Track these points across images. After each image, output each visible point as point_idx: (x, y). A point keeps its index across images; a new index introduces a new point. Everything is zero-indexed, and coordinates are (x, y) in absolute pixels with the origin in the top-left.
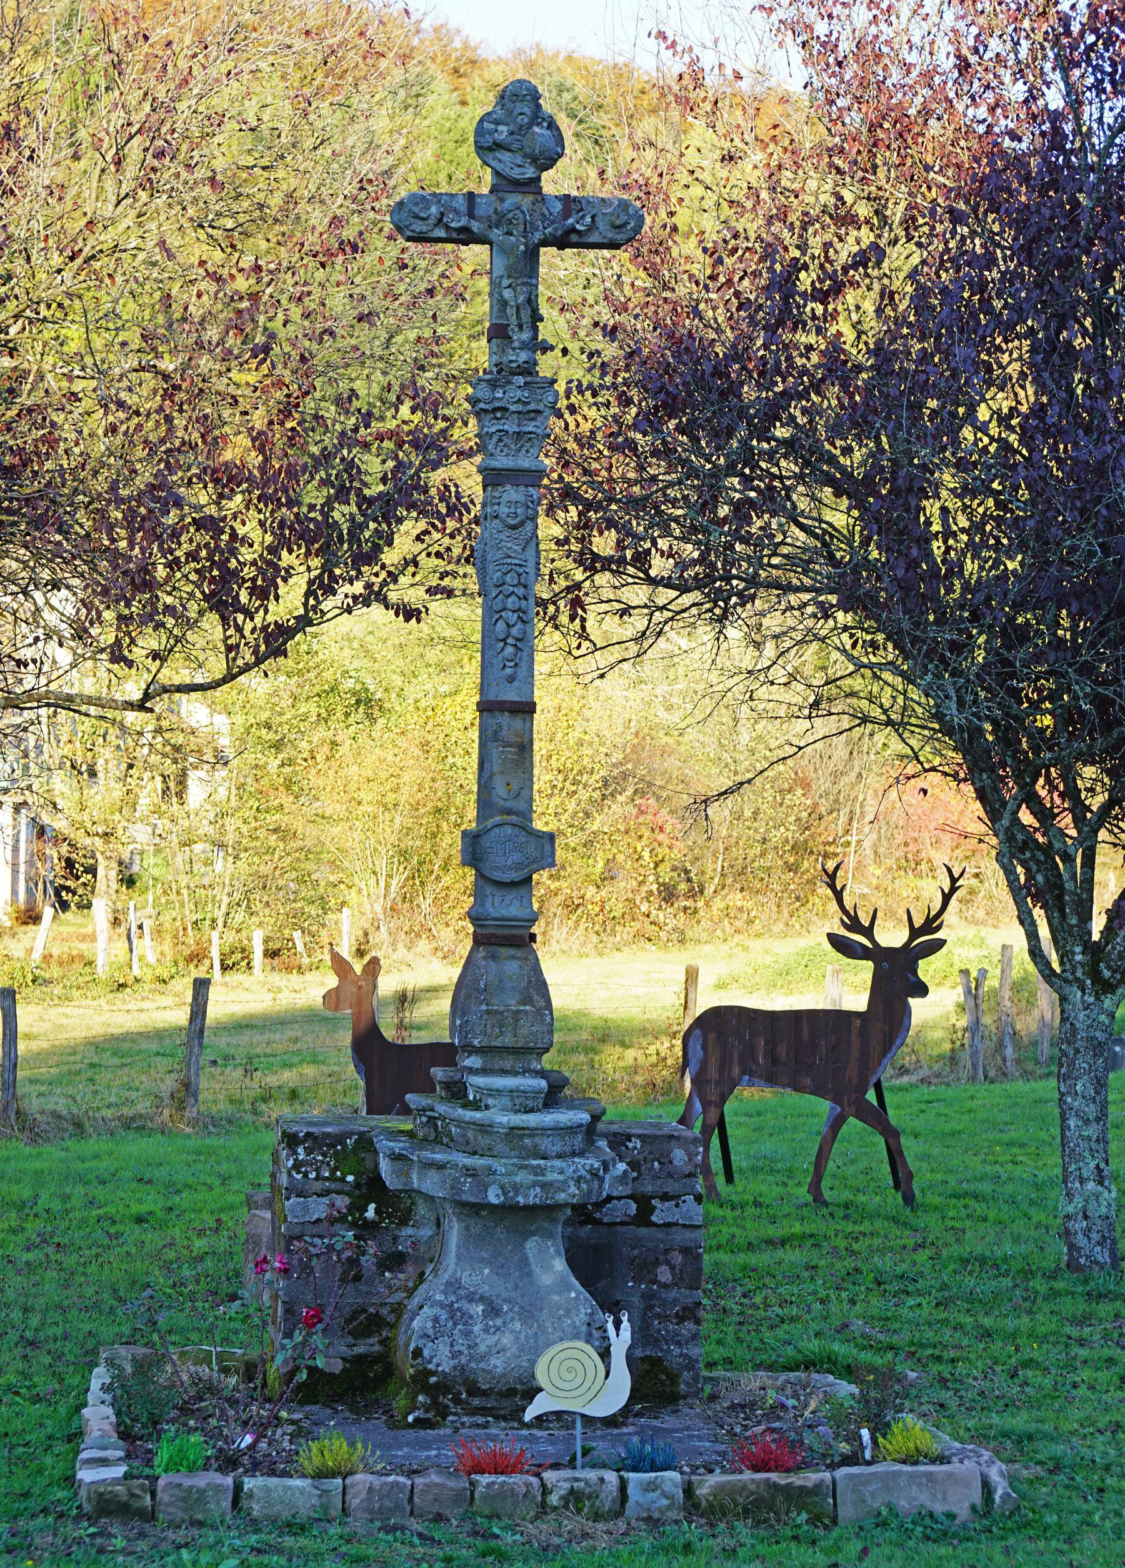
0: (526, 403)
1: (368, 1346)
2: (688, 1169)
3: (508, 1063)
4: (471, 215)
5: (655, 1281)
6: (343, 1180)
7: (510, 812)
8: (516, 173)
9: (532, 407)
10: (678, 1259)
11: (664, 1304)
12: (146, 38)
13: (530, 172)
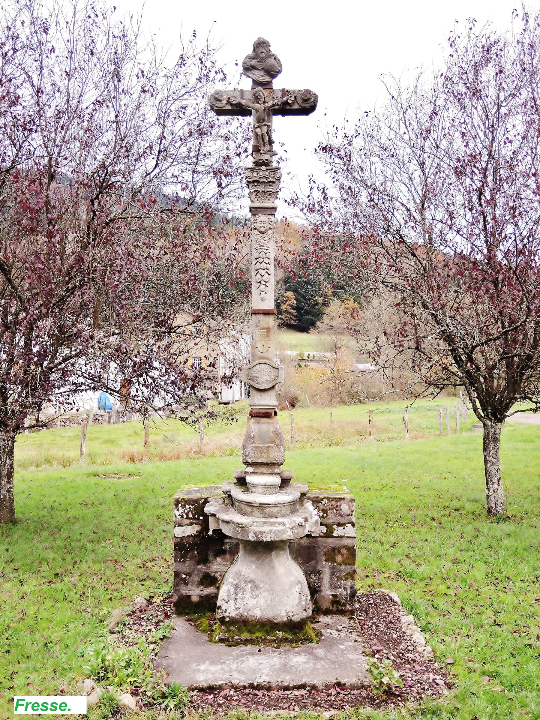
0: (267, 178)
1: (209, 591)
2: (349, 512)
3: (264, 470)
4: (242, 97)
5: (335, 562)
6: (198, 518)
7: (263, 358)
8: (261, 79)
9: (270, 180)
10: (344, 551)
11: (340, 571)
12: (534, 582)
13: (267, 79)
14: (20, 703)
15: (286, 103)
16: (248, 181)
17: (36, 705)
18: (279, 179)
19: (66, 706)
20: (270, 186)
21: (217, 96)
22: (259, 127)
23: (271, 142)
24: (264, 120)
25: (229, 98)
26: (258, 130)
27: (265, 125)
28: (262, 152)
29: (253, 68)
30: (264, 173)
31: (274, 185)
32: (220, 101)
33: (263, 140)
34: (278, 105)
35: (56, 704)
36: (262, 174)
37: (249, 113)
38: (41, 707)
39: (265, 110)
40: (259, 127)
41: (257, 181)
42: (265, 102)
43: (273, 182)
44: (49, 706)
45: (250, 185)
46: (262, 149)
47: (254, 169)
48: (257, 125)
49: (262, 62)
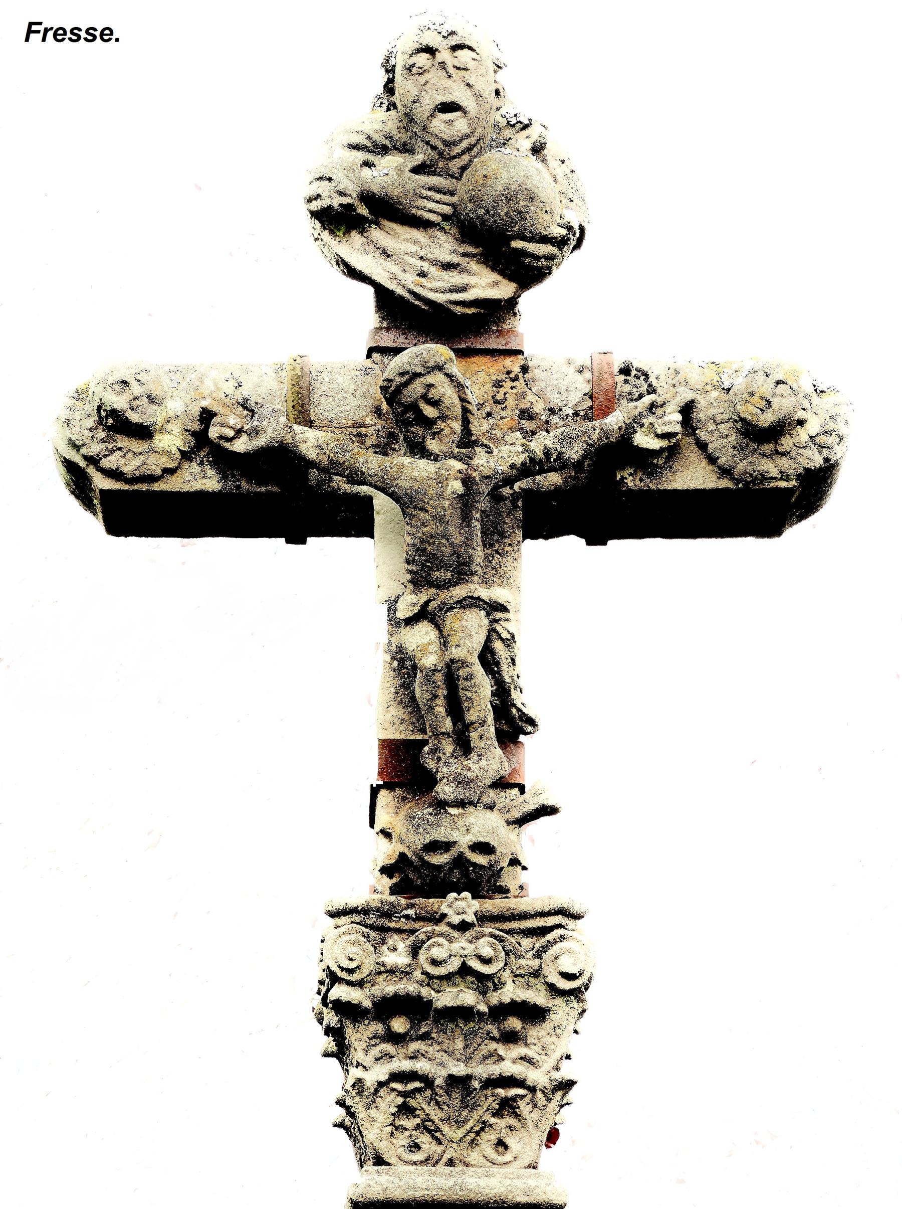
0: (485, 983)
8: (437, 288)
9: (510, 992)
13: (486, 284)
14: (34, 28)
15: (620, 451)
16: (340, 1007)
17: (61, 32)
18: (574, 990)
19: (112, 33)
20: (510, 1038)
21: (119, 402)
22: (423, 614)
23: (512, 726)
24: (462, 571)
25: (207, 416)
26: (421, 637)
27: (472, 602)
28: (445, 790)
29: (383, 209)
30: (462, 945)
31: (535, 1033)
32: (144, 432)
33: (456, 708)
34: (561, 464)
35: (95, 30)
36: (450, 950)
37: (355, 520)
38: (69, 35)
39: (466, 501)
40: (423, 614)
41: (414, 1007)
42: (467, 441)
43: (534, 1014)
44: (83, 34)
45: (358, 1036)
46: (446, 765)
47: (387, 913)
48: (407, 606)
49: (452, 218)
